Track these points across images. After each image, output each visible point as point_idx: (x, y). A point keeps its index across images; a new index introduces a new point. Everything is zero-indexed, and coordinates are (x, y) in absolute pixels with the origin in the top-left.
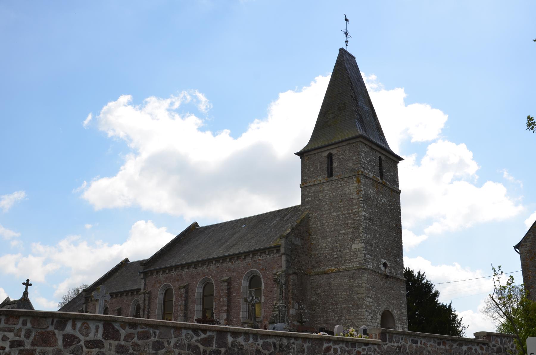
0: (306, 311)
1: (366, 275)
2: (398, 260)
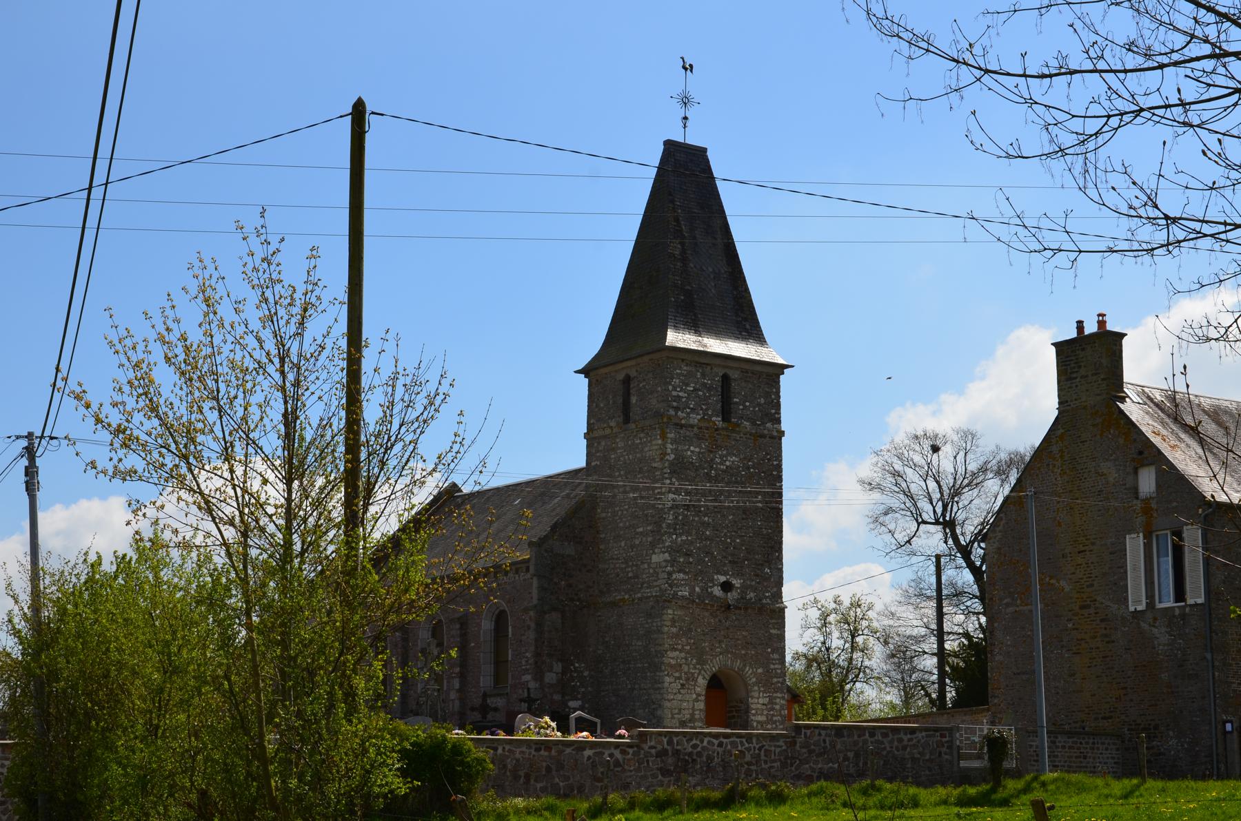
0: (586, 674)
1: (670, 611)
2: (767, 570)
